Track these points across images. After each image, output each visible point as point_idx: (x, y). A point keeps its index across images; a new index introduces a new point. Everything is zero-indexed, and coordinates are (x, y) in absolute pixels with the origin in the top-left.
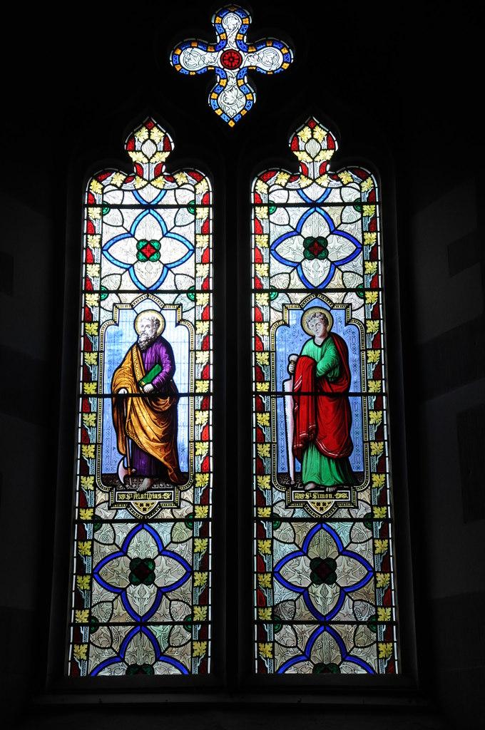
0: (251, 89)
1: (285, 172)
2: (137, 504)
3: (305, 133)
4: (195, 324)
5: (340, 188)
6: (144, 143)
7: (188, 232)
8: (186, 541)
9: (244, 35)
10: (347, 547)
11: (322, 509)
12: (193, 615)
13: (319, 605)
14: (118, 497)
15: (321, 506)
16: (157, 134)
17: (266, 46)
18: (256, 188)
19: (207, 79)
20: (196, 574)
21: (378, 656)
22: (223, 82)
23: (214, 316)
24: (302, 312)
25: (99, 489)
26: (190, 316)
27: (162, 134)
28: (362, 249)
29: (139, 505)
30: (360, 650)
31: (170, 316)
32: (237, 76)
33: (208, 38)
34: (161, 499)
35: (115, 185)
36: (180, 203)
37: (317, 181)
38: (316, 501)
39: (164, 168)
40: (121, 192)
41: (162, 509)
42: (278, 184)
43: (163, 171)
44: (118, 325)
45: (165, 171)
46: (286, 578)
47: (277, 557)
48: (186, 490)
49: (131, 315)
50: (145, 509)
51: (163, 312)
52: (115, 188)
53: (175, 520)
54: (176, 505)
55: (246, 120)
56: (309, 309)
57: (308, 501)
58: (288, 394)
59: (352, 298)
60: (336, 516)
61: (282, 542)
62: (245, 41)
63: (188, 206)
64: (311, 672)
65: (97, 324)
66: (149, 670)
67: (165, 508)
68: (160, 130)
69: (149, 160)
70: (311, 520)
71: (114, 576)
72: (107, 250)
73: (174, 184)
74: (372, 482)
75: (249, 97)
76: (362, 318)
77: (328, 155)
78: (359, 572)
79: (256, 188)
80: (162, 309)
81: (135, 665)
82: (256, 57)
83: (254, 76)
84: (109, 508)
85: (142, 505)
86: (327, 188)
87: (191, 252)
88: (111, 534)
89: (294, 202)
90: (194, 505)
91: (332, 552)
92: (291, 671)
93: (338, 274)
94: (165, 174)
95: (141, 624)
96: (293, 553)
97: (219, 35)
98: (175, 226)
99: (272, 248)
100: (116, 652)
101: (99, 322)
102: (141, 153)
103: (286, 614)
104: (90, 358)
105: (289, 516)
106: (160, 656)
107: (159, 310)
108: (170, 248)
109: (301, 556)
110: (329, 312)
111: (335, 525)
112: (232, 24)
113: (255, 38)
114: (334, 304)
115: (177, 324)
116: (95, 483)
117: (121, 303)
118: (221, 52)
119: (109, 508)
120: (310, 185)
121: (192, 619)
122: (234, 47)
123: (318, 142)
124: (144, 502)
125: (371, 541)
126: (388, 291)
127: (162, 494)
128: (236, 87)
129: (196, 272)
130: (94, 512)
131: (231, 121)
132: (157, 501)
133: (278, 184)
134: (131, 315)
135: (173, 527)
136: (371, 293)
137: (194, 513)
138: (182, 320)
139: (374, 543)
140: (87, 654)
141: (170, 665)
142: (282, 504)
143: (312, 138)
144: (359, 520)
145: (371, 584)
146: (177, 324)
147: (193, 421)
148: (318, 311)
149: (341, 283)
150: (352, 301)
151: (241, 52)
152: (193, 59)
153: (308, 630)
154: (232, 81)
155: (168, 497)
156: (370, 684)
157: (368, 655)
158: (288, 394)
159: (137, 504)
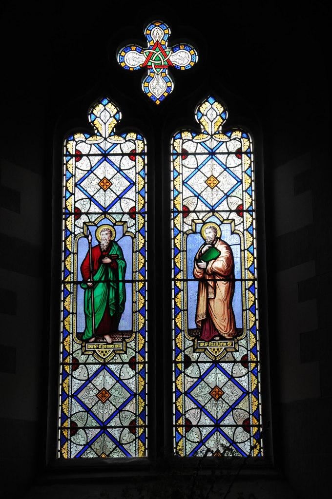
0: (170, 79)
2: (211, 349)
3: (205, 107)
9: (166, 41)
11: (104, 355)
14: (199, 345)
15: (104, 353)
19: (142, 72)
23: (170, 231)
24: (96, 228)
26: (240, 228)
33: (141, 42)
34: (114, 348)
38: (212, 348)
50: (216, 352)
55: (168, 100)
56: (102, 225)
57: (208, 347)
58: (238, 280)
63: (129, 155)
72: (186, 183)
76: (134, 232)
83: (174, 71)
85: (214, 350)
89: (117, 157)
97: (149, 42)
99: (241, 182)
110: (219, 226)
112: (158, 33)
113: (174, 43)
124: (216, 348)
127: (227, 343)
131: (158, 101)
132: (224, 347)
148: (106, 227)
152: (132, 59)
155: (230, 345)
156: (128, 466)
158: (238, 280)
159: (211, 349)
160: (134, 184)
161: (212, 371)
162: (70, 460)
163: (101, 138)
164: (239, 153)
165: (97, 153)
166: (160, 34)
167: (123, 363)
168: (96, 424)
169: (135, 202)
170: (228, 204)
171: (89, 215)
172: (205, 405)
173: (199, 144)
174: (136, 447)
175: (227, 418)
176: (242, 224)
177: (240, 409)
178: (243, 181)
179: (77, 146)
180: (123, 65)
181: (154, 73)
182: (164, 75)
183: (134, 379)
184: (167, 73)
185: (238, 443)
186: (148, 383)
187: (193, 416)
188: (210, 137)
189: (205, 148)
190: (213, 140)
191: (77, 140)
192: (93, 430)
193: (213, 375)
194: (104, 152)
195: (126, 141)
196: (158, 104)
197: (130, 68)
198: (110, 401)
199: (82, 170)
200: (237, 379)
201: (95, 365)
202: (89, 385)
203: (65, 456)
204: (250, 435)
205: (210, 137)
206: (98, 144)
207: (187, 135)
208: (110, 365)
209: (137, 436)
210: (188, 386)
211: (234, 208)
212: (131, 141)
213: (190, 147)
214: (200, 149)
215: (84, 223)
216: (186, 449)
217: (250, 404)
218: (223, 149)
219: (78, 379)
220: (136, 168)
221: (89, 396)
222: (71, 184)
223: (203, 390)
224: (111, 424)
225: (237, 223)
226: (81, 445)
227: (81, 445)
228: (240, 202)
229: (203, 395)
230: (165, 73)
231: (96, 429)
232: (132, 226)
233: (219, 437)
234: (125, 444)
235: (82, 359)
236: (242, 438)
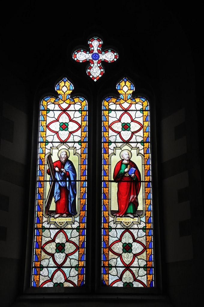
1: (54, 98)
4: (81, 155)
5: (135, 104)
6: (63, 87)
7: (141, 120)
8: (143, 236)
10: (69, 239)
12: (79, 264)
13: (125, 260)
17: (108, 52)
18: (43, 103)
19: (87, 64)
20: (147, 249)
21: (147, 280)
22: (92, 65)
25: (44, 216)
27: (130, 84)
28: (81, 127)
30: (72, 278)
31: (71, 151)
32: (97, 62)
33: (87, 49)
35: (52, 102)
37: (127, 101)
39: (70, 96)
40: (115, 105)
41: (68, 224)
42: (51, 102)
43: (69, 97)
44: (115, 155)
45: (70, 98)
46: (113, 250)
47: (43, 243)
48: (77, 217)
49: (57, 151)
51: (69, 150)
52: (113, 103)
53: (139, 229)
54: (73, 223)
55: (118, 80)
59: (139, 145)
60: (66, 227)
61: (114, 235)
62: (100, 50)
64: (53, 286)
65: (44, 154)
66: (61, 285)
67: (135, 224)
68: (129, 82)
69: (64, 93)
70: (57, 229)
71: (117, 249)
73: (74, 102)
74: (146, 214)
75: (102, 70)
77: (131, 92)
78: (141, 248)
79: (43, 103)
80: (69, 149)
81: (57, 283)
82: (105, 56)
83: (104, 64)
84: (48, 224)
86: (69, 104)
87: (142, 127)
88: (49, 234)
90: (145, 223)
91: (131, 241)
92: (46, 286)
93: (72, 136)
94: (70, 98)
95: (128, 267)
96: (116, 241)
98: (74, 117)
100: (50, 278)
101: (45, 153)
102: (122, 90)
103: (113, 263)
104: (106, 167)
105: (48, 227)
106: (135, 280)
107: (68, 149)
108: (118, 126)
109: (119, 242)
111: (131, 230)
112: (95, 44)
113: (104, 49)
114: (70, 147)
115: (137, 155)
116: (43, 214)
117: (53, 147)
118: (92, 54)
119: (48, 224)
120: (63, 103)
121: (78, 266)
122: (97, 52)
123: (127, 87)
125: (145, 236)
126: (152, 142)
128: (97, 66)
129: (144, 135)
130: (42, 225)
133: (51, 102)
134: (57, 151)
135: (72, 231)
136: (83, 143)
137: (146, 226)
138: (139, 153)
139: (146, 237)
140: (39, 278)
141: (138, 283)
142: (46, 223)
143: (125, 85)
144: (141, 229)
145: (77, 252)
146: (137, 155)
147: (44, 190)
149: (135, 140)
150: (77, 146)
151: (99, 54)
152: (81, 56)
153: (122, 269)
154: (96, 64)
157: (74, 280)
164: (142, 111)
165: (120, 109)
180: (76, 59)
184: (101, 64)
189: (121, 108)
196: (95, 81)
197: (108, 61)
225: (77, 148)
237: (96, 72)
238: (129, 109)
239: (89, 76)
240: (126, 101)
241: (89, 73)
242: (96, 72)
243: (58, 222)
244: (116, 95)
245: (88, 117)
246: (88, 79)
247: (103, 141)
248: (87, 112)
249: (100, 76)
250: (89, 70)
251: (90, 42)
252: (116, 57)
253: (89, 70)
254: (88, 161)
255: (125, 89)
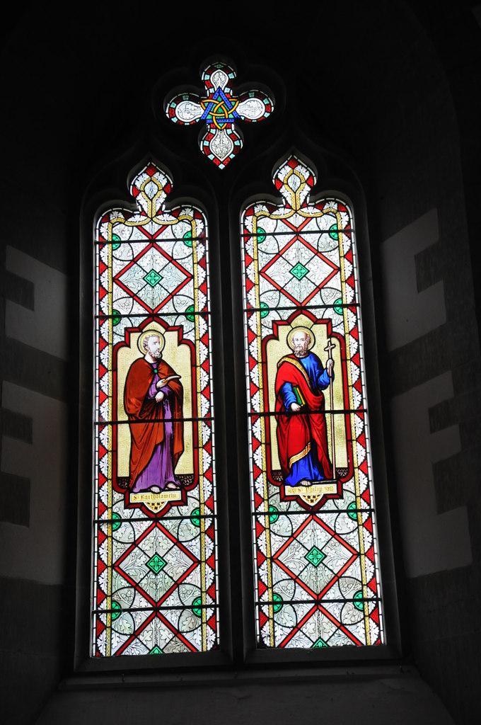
3: (141, 181)
16: (161, 179)
19: (199, 128)
29: (151, 504)
33: (198, 93)
36: (322, 229)
56: (148, 331)
76: (342, 332)
83: (243, 125)
99: (115, 280)
112: (220, 79)
113: (240, 90)
152: (187, 112)
156: (355, 656)
159: (149, 503)
160: (191, 277)
161: (151, 533)
162: (272, 649)
163: (146, 218)
166: (223, 79)
167: (339, 512)
168: (146, 604)
169: (194, 300)
170: (174, 305)
171: (131, 318)
172: (139, 582)
173: (279, 221)
174: (202, 635)
175: (331, 590)
176: (193, 331)
177: (189, 584)
178: (257, 274)
179: (258, 222)
180: (174, 120)
181: (216, 128)
182: (229, 131)
183: (198, 540)
184: (233, 129)
185: (346, 624)
186: (218, 545)
187: (126, 597)
188: (149, 220)
190: (298, 215)
191: (113, 222)
192: (305, 605)
193: (310, 532)
194: (295, 230)
195: (179, 221)
198: (324, 564)
199: (121, 260)
200: (184, 544)
201: (301, 515)
202: (135, 550)
203: (102, 650)
204: (364, 614)
205: (149, 220)
206: (285, 219)
207: (261, 209)
208: (164, 521)
209: (367, 614)
210: (117, 555)
211: (182, 310)
212: (330, 213)
213: (268, 225)
214: (282, 227)
215: (274, 322)
216: (111, 644)
217: (203, 577)
218: (312, 226)
219: (120, 542)
220: (193, 255)
221: (294, 559)
222: (347, 268)
223: (297, 553)
224: (328, 596)
226: (126, 635)
227: (126, 635)
228: (191, 303)
229: (296, 560)
230: (231, 128)
231: (146, 612)
232: (339, 325)
233: (159, 626)
234: (187, 632)
235: (125, 514)
236: (191, 626)
237: (221, 146)
238: (302, 230)
239: (206, 157)
240: (301, 309)
241: (207, 148)
242: (221, 146)
243: (149, 503)
244: (273, 197)
245: (219, 563)
246: (205, 163)
247: (242, 233)
248: (218, 609)
249: (232, 156)
250: (206, 143)
251: (207, 77)
252: (268, 107)
253: (206, 143)
254: (210, 292)
255: (294, 181)
